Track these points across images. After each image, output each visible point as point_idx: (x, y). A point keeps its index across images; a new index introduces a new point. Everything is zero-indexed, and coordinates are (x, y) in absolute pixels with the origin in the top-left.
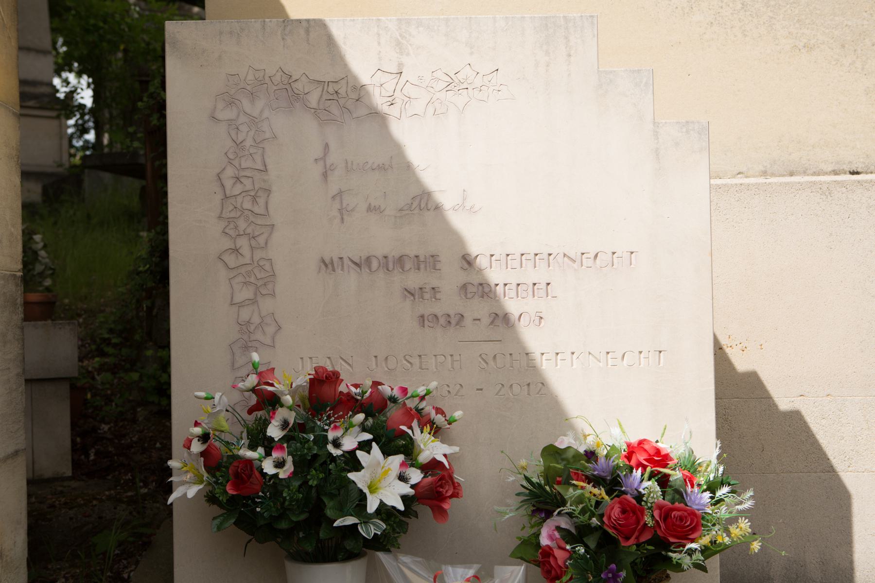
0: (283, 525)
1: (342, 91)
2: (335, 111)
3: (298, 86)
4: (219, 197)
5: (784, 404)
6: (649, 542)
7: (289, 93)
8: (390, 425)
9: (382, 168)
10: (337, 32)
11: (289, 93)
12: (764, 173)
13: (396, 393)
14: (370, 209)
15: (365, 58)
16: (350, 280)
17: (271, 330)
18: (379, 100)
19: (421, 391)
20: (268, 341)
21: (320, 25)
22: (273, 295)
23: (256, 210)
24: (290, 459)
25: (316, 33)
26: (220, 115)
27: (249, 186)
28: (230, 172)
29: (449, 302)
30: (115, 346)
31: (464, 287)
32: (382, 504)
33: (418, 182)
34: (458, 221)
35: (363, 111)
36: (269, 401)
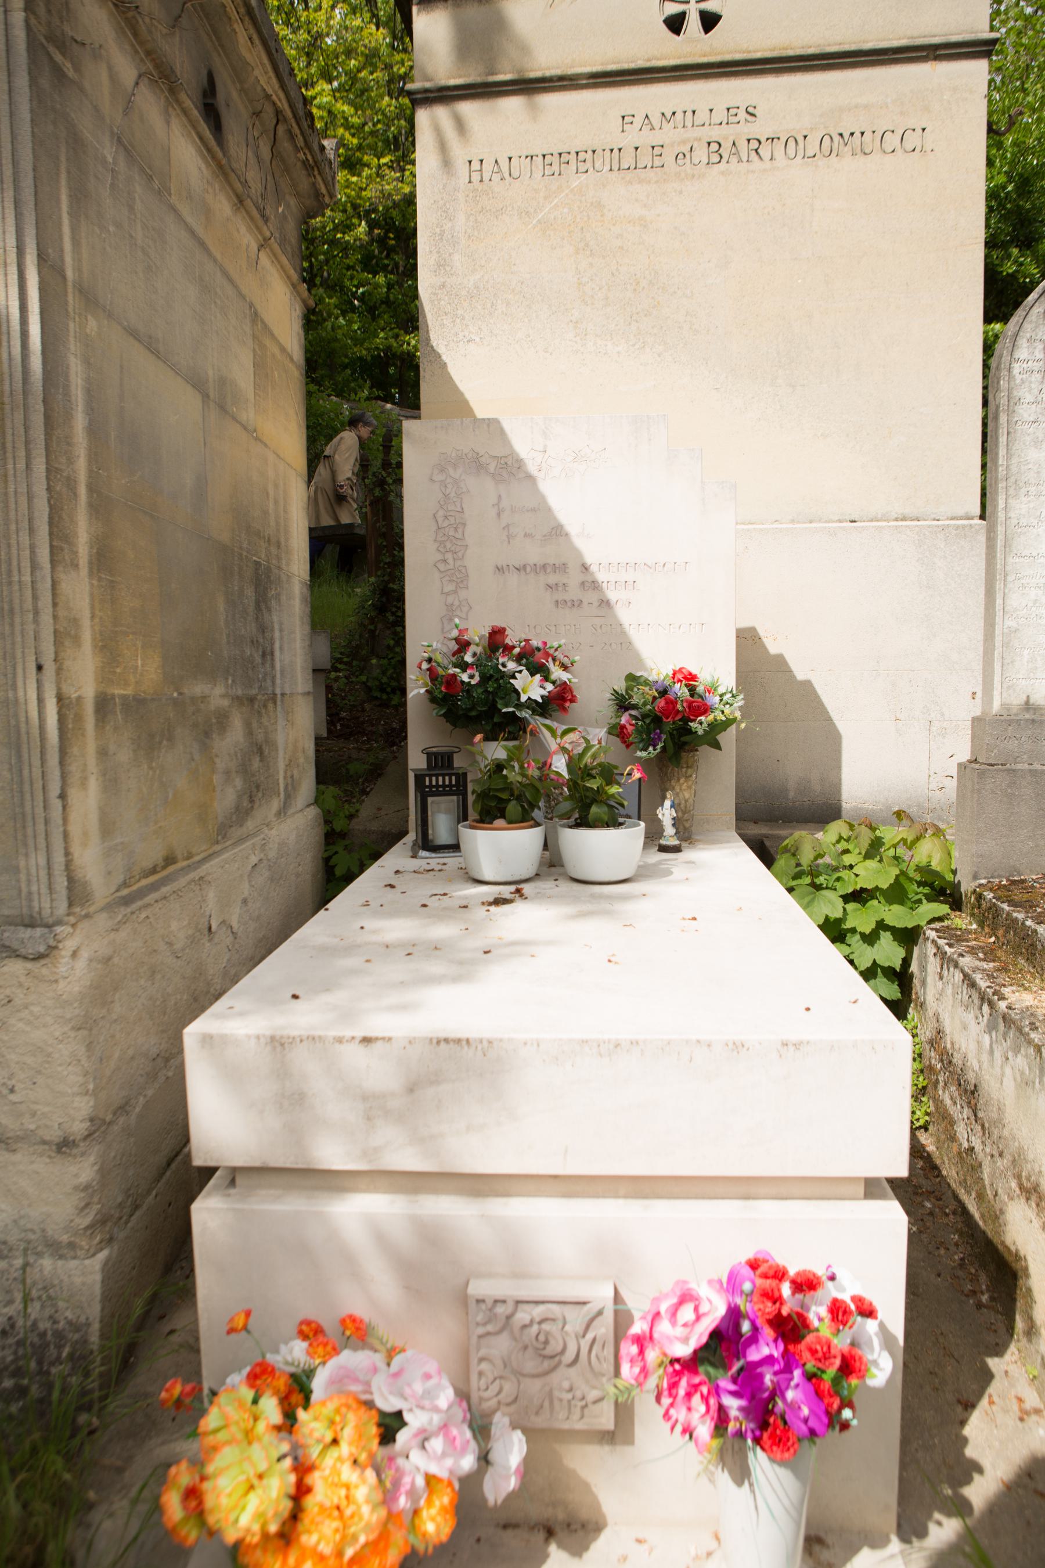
0: (473, 713)
1: (509, 463)
2: (505, 474)
3: (483, 460)
4: (435, 528)
5: (800, 676)
6: (680, 720)
7: (477, 464)
8: (534, 661)
9: (534, 510)
10: (506, 426)
11: (477, 464)
12: (793, 521)
13: (540, 645)
14: (526, 535)
15: (524, 444)
16: (513, 579)
17: (465, 609)
18: (532, 468)
19: (555, 644)
20: (464, 616)
21: (496, 421)
22: (467, 588)
23: (457, 536)
24: (477, 674)
25: (493, 426)
26: (435, 478)
27: (453, 521)
28: (441, 513)
29: (574, 592)
30: (346, 663)
31: (583, 583)
32: (529, 698)
33: (555, 518)
34: (579, 543)
35: (522, 475)
36: (463, 645)
